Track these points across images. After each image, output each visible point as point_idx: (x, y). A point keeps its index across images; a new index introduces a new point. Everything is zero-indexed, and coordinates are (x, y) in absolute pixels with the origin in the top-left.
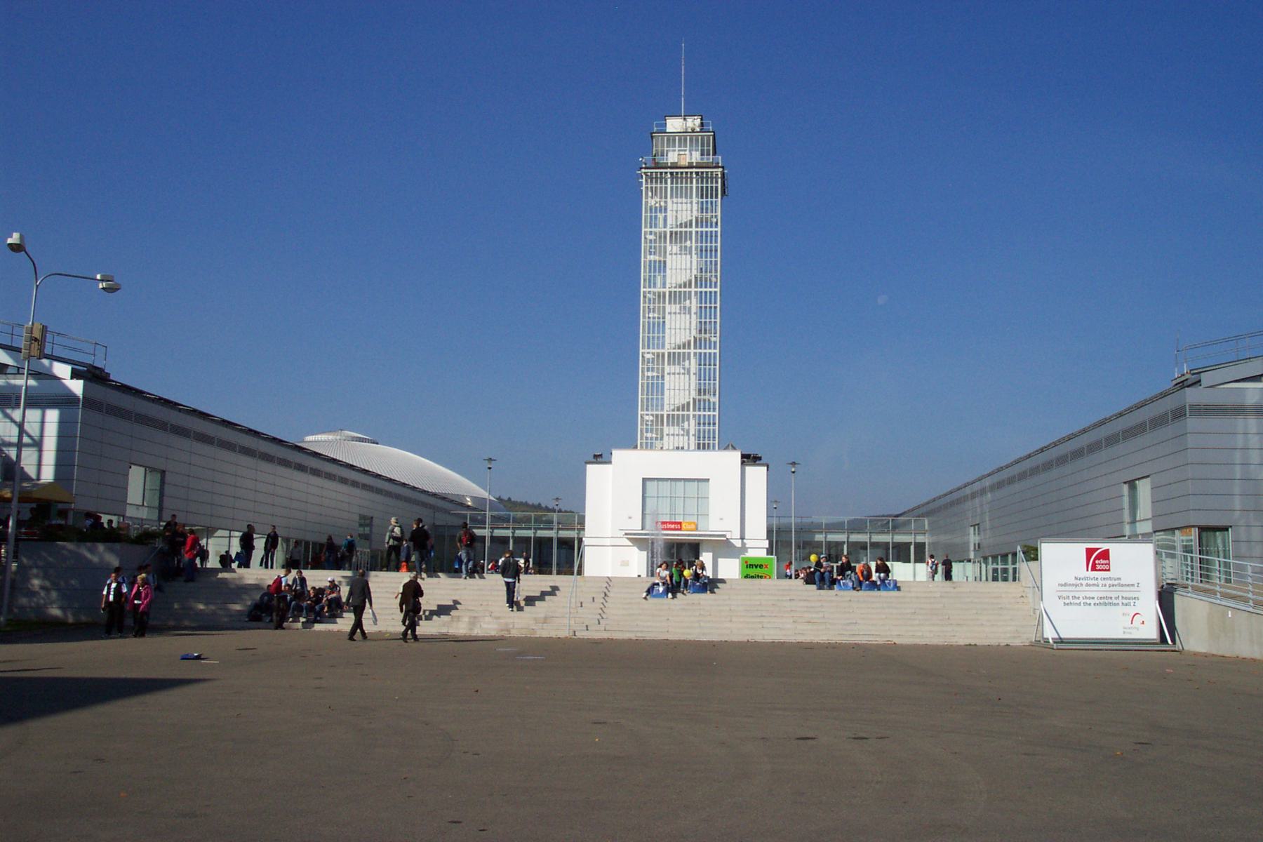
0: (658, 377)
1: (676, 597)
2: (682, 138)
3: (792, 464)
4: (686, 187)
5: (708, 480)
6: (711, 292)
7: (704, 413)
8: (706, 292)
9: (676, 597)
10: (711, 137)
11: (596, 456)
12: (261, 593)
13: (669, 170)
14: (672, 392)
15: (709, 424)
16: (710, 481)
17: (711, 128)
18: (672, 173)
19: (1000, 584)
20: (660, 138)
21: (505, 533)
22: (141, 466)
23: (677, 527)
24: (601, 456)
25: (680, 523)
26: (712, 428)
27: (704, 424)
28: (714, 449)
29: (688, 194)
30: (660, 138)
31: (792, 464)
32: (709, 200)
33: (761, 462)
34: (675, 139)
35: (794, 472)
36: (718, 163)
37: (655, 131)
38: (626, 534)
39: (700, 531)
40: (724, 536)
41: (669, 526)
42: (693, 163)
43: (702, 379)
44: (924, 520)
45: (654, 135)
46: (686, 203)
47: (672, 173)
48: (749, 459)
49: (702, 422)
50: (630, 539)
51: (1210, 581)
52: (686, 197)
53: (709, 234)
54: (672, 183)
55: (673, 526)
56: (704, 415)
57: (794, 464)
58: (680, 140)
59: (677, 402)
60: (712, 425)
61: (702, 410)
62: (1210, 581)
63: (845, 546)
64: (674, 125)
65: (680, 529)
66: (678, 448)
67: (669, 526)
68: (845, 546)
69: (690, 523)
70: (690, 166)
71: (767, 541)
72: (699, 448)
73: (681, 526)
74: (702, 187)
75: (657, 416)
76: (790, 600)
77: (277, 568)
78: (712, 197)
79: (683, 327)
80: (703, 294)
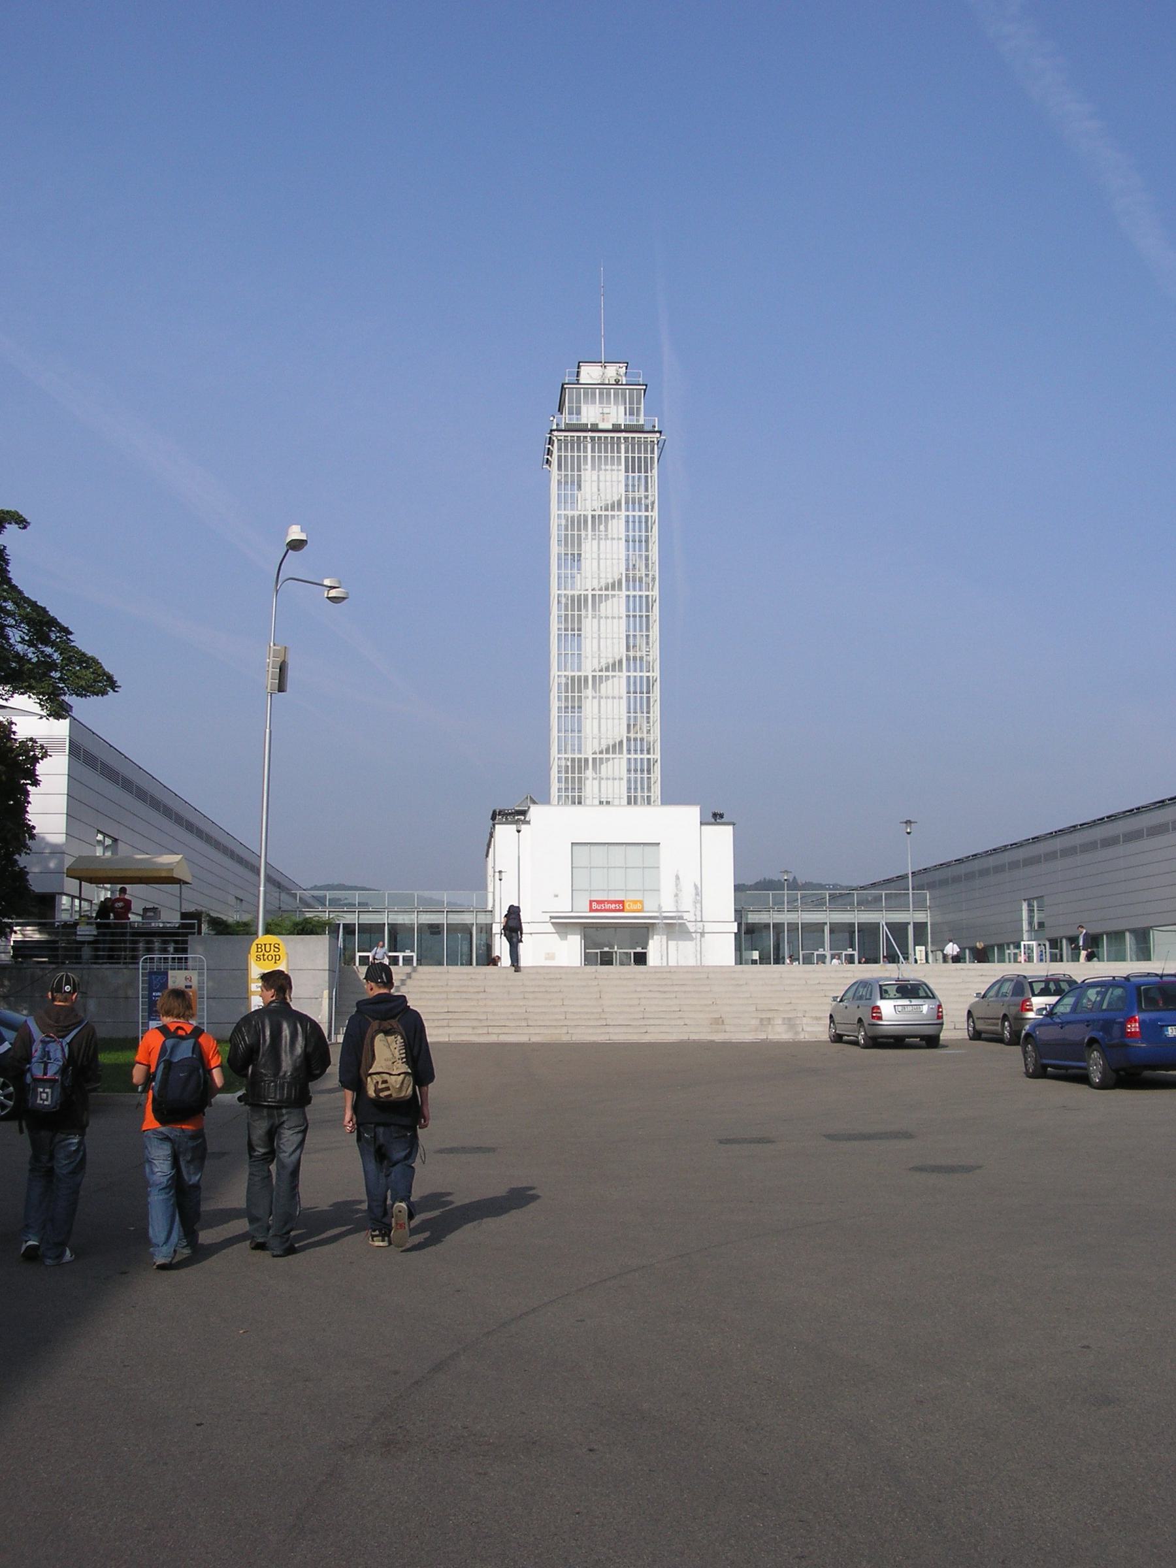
0: (566, 707)
2: (603, 391)
3: (906, 823)
5: (659, 844)
6: (641, 597)
7: (636, 756)
8: (634, 596)
10: (643, 391)
11: (715, 815)
12: (348, 1018)
13: (590, 434)
15: (642, 771)
16: (660, 845)
17: (641, 379)
18: (593, 439)
19: (773, 967)
20: (597, 390)
21: (376, 919)
22: (491, 835)
23: (618, 906)
25: (622, 902)
26: (639, 776)
27: (636, 771)
28: (635, 803)
30: (612, 390)
31: (906, 823)
32: (643, 474)
33: (723, 820)
34: (610, 392)
35: (909, 833)
36: (654, 427)
37: (567, 382)
38: (551, 918)
39: (645, 912)
40: (681, 918)
41: (608, 906)
42: (620, 425)
43: (632, 711)
44: (926, 893)
45: (565, 386)
47: (593, 439)
48: (717, 818)
49: (633, 768)
51: (81, 961)
53: (631, 520)
54: (593, 451)
55: (613, 906)
56: (636, 759)
57: (908, 822)
58: (601, 394)
60: (639, 772)
61: (632, 752)
62: (81, 961)
63: (474, 928)
64: (590, 374)
65: (623, 910)
66: (601, 803)
67: (608, 906)
68: (474, 928)
69: (635, 902)
70: (616, 429)
71: (736, 924)
72: (629, 803)
73: (623, 906)
74: (633, 458)
75: (573, 760)
76: (959, 995)
78: (633, 472)
80: (631, 598)
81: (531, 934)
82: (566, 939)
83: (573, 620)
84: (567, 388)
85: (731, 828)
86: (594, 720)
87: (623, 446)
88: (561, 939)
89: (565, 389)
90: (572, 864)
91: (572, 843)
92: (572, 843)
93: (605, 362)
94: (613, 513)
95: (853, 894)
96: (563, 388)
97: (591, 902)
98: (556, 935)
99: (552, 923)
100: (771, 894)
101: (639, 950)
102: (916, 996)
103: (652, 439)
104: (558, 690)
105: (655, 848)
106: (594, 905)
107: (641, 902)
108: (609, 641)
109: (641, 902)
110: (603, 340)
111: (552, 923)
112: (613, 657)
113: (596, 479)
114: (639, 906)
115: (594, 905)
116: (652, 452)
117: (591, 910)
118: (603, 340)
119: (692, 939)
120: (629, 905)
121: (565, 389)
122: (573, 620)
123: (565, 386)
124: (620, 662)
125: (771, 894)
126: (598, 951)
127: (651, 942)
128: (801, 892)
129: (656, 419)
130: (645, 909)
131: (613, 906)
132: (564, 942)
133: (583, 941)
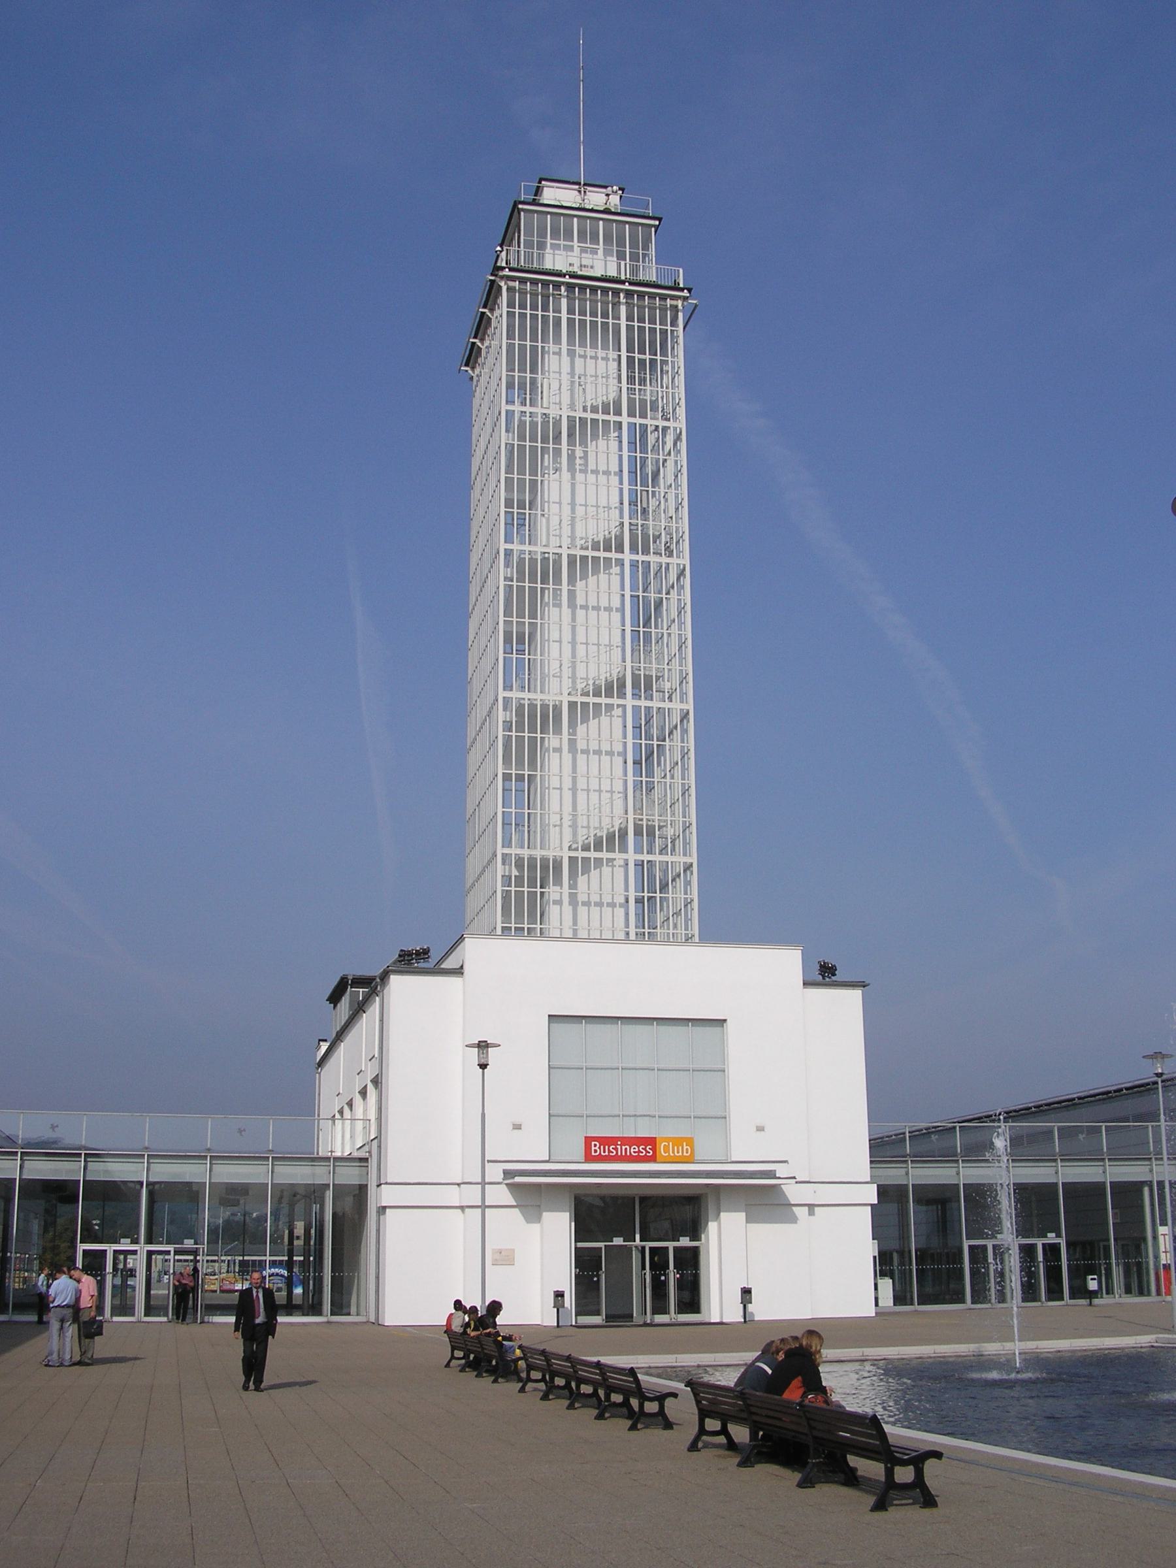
1: (814, 1214)
4: (534, 317)
9: (814, 1214)
14: (594, 797)
16: (728, 1021)
24: (424, 954)
25: (651, 1141)
29: (606, 335)
30: (575, 220)
38: (508, 1174)
40: (771, 1174)
41: (623, 1149)
45: (520, 206)
46: (606, 359)
50: (513, 1187)
52: (605, 347)
59: (594, 822)
65: (653, 1159)
67: (623, 1149)
69: (678, 1141)
73: (654, 1149)
77: (516, 847)
78: (642, 351)
79: (605, 640)
81: (462, 1208)
82: (538, 1219)
83: (521, 490)
84: (523, 210)
85: (856, 995)
86: (585, 824)
87: (623, 309)
88: (528, 1222)
89: (519, 211)
90: (549, 1062)
91: (549, 1016)
92: (549, 1016)
93: (585, 185)
94: (609, 701)
95: (1147, 1127)
96: (515, 210)
97: (588, 1140)
98: (517, 1210)
99: (506, 1184)
100: (1104, 1128)
101: (685, 1242)
102: (772, 1176)
103: (674, 302)
104: (605, 1141)
105: (716, 1030)
106: (595, 1148)
107: (690, 1141)
108: (606, 785)
109: (690, 1141)
110: (582, 147)
111: (506, 1184)
112: (611, 716)
113: (578, 507)
114: (685, 1150)
115: (595, 1148)
116: (674, 323)
117: (589, 1158)
118: (582, 147)
119: (793, 1219)
120: (666, 1149)
121: (519, 211)
122: (521, 490)
123: (520, 206)
124: (623, 833)
125: (1104, 1128)
126: (601, 1245)
127: (712, 1226)
128: (1152, 1124)
129: (681, 271)
130: (697, 1158)
131: (634, 1149)
132: (535, 1227)
133: (573, 1224)
